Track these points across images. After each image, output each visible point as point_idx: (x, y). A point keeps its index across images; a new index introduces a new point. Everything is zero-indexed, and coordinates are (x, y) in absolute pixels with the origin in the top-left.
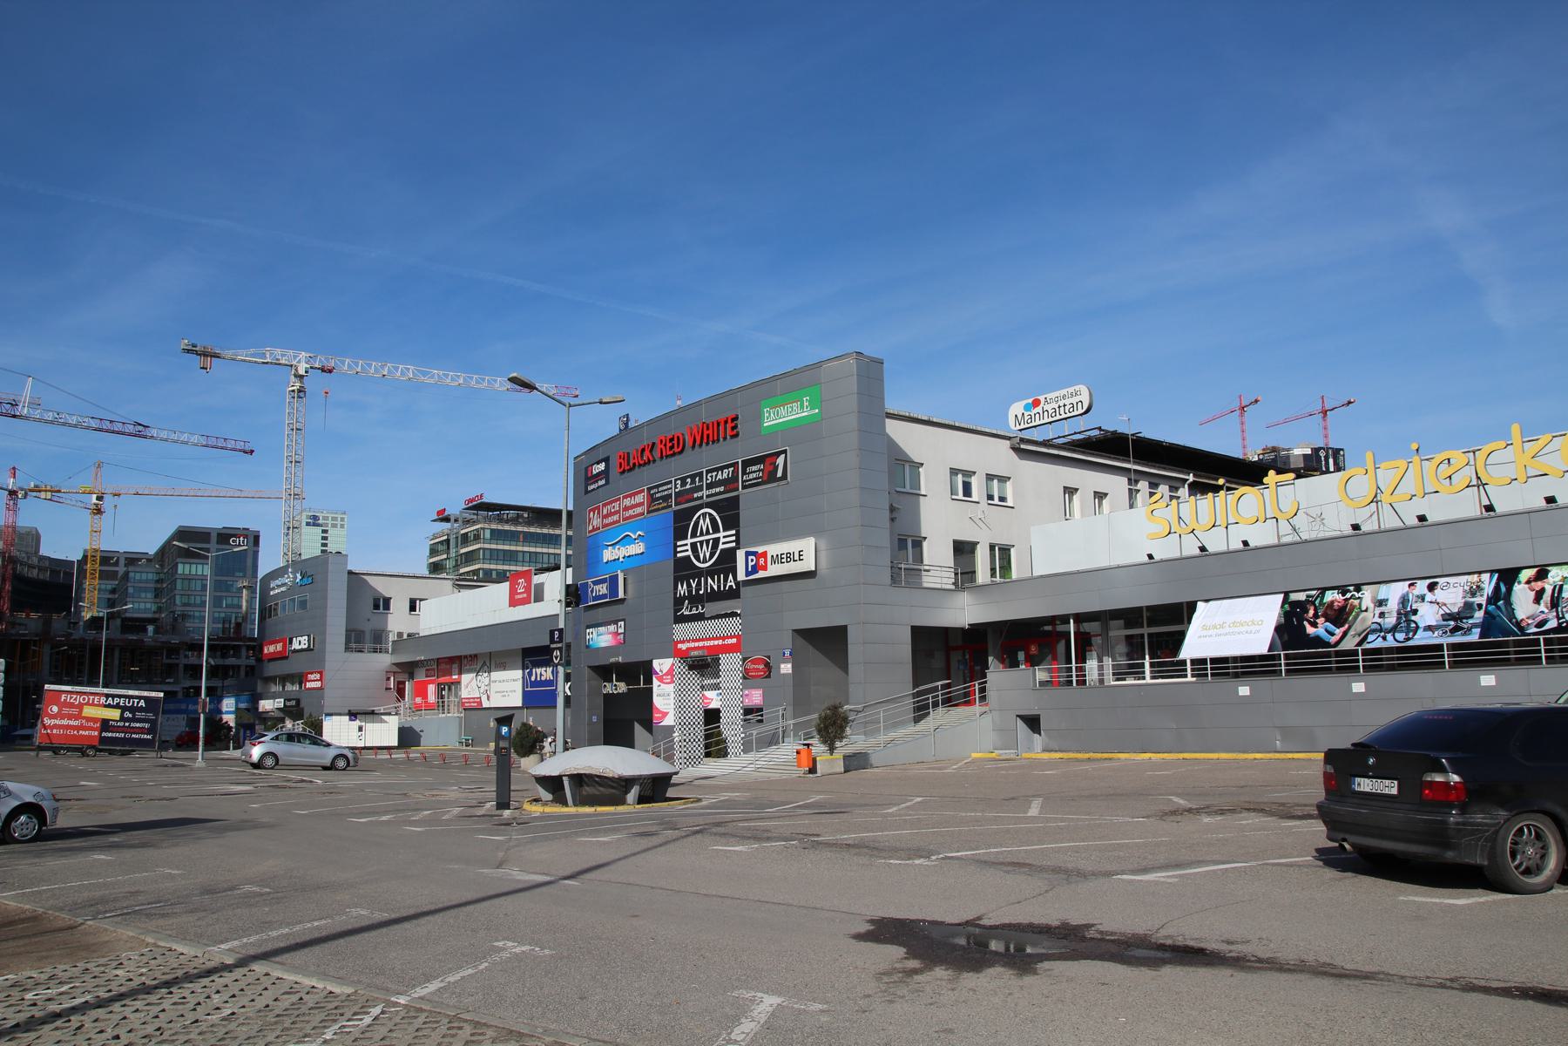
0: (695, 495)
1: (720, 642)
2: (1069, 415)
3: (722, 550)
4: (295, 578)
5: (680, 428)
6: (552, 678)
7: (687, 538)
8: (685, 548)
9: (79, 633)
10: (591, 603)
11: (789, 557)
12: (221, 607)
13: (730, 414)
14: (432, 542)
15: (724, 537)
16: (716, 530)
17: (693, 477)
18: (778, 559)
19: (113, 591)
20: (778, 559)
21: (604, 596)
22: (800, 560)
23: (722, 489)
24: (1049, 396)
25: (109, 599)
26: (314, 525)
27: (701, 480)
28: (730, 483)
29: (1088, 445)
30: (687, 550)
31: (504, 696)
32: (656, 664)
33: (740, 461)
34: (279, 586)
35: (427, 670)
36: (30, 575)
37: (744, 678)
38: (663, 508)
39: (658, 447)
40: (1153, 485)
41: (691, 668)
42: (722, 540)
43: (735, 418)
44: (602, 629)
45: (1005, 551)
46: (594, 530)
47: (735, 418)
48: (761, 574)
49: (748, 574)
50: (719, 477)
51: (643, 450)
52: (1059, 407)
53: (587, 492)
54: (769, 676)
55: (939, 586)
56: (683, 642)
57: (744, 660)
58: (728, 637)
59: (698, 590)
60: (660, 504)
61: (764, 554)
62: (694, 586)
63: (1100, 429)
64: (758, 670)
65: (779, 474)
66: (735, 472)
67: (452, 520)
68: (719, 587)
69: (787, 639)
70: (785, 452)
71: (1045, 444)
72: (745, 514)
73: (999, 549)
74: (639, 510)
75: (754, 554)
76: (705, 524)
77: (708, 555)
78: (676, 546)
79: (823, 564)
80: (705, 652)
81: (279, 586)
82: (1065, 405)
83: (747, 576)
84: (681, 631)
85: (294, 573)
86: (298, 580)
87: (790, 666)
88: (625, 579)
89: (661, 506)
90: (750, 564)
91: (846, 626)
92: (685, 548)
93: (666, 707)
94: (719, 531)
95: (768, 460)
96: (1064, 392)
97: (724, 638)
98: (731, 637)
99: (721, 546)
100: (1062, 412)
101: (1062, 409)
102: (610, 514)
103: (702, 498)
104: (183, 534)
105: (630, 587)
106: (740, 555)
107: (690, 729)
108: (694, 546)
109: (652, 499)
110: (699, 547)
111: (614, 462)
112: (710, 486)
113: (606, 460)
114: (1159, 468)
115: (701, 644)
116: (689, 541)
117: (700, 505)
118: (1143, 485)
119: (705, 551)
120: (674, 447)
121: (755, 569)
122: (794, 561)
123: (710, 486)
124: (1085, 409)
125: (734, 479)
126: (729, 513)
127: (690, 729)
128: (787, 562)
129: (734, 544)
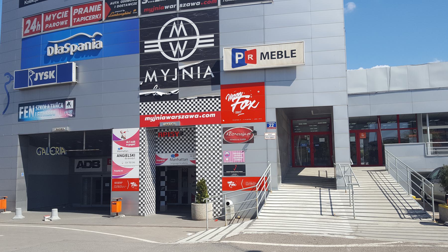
6: (53, 77)
7: (156, 38)
10: (32, 86)
15: (200, 39)
21: (52, 80)
22: (292, 56)
30: (158, 48)
32: (116, 132)
42: (198, 41)
49: (234, 65)
60: (123, 12)
62: (165, 74)
68: (195, 76)
78: (143, 45)
80: (178, 124)
88: (76, 67)
89: (123, 14)
90: (237, 59)
91: (332, 106)
93: (129, 164)
99: (197, 46)
103: (175, 9)
105: (80, 74)
107: (214, 194)
121: (242, 63)
122: (286, 57)
127: (214, 194)
128: (278, 58)
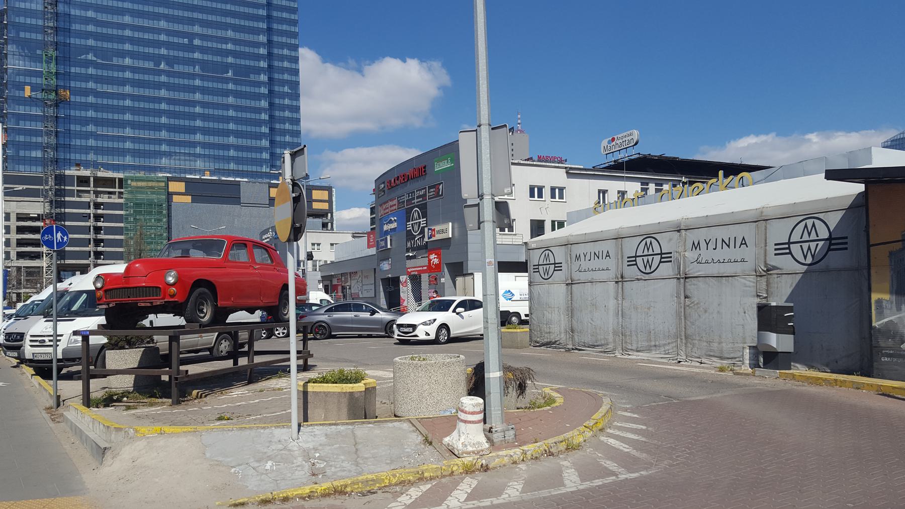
1: (421, 268)
2: (627, 146)
4: (273, 234)
13: (423, 165)
14: (371, 206)
16: (420, 219)
17: (412, 193)
18: (439, 232)
20: (439, 232)
21: (383, 247)
23: (421, 199)
24: (619, 136)
27: (414, 195)
29: (610, 168)
31: (367, 292)
34: (266, 239)
35: (338, 279)
37: (429, 284)
40: (659, 184)
42: (422, 223)
44: (385, 262)
47: (425, 167)
49: (429, 238)
52: (623, 142)
53: (379, 198)
55: (511, 243)
56: (409, 268)
57: (429, 276)
65: (440, 194)
66: (426, 191)
71: (594, 169)
73: (558, 222)
74: (394, 207)
75: (431, 229)
76: (416, 215)
79: (456, 234)
81: (266, 239)
82: (625, 141)
83: (428, 239)
84: (410, 263)
90: (430, 234)
94: (420, 219)
95: (436, 186)
96: (625, 134)
97: (422, 267)
99: (421, 226)
100: (624, 145)
101: (624, 142)
105: (393, 242)
106: (426, 229)
109: (399, 203)
112: (418, 198)
113: (384, 183)
115: (415, 269)
116: (411, 223)
117: (414, 206)
119: (416, 228)
123: (418, 198)
124: (634, 143)
125: (425, 195)
129: (425, 225)
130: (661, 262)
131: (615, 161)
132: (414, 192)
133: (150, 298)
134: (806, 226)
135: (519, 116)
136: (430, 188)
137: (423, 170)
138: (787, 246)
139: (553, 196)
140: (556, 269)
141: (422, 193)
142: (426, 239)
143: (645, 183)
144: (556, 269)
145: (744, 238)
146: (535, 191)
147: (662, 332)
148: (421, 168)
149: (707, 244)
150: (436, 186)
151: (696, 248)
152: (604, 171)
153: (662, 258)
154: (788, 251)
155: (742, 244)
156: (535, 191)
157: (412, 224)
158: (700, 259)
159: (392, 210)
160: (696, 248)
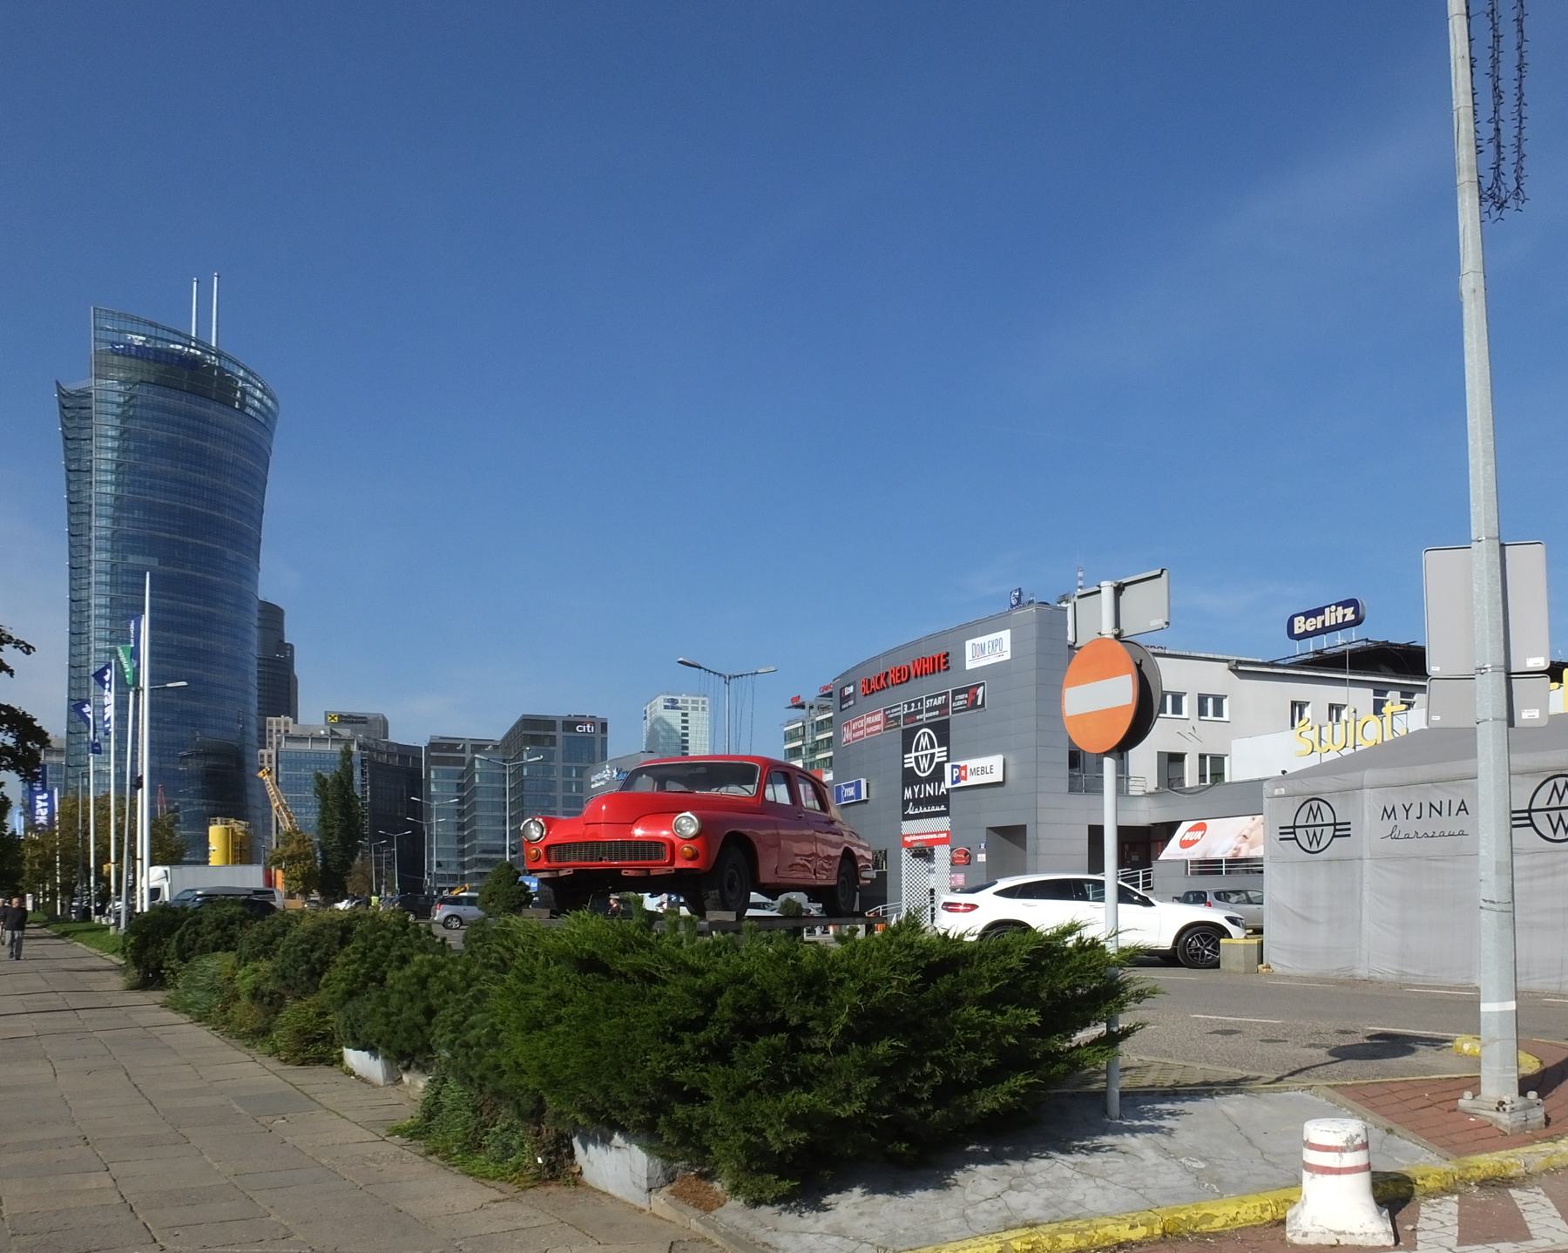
0: (918, 717)
3: (937, 763)
4: (612, 773)
5: (905, 661)
7: (911, 752)
8: (910, 761)
9: (1050, 1003)
11: (983, 771)
12: (571, 791)
16: (933, 746)
17: (916, 702)
19: (461, 777)
21: (852, 798)
23: (937, 713)
25: (458, 784)
26: (673, 708)
27: (922, 705)
28: (944, 706)
33: (950, 690)
36: (380, 760)
37: (952, 864)
38: (895, 727)
39: (891, 676)
41: (914, 856)
42: (937, 755)
43: (947, 655)
45: (1218, 761)
46: (847, 742)
47: (947, 655)
48: (963, 783)
49: (953, 783)
50: (935, 703)
51: (879, 678)
53: (841, 710)
54: (969, 864)
56: (908, 835)
57: (952, 850)
58: (941, 832)
59: (919, 795)
61: (965, 768)
63: (1367, 640)
64: (961, 859)
65: (979, 703)
67: (807, 706)
69: (983, 833)
70: (983, 684)
71: (1272, 664)
72: (954, 735)
74: (877, 727)
75: (958, 767)
76: (924, 741)
77: (926, 767)
78: (903, 759)
84: (908, 827)
85: (610, 769)
86: (614, 776)
87: (984, 855)
90: (955, 775)
92: (910, 761)
95: (970, 690)
97: (937, 833)
98: (943, 832)
99: (936, 760)
102: (858, 730)
104: (528, 722)
106: (948, 767)
108: (916, 758)
109: (887, 719)
110: (920, 759)
111: (860, 686)
112: (928, 710)
114: (1412, 679)
116: (913, 754)
118: (1393, 696)
119: (924, 763)
120: (903, 676)
121: (958, 779)
123: (928, 710)
126: (942, 732)
130: (1334, 836)
131: (1316, 652)
132: (921, 700)
133: (650, 862)
134: (1555, 787)
135: (1080, 574)
136: (956, 693)
137: (942, 660)
138: (1292, 830)
139: (1202, 711)
140: (1337, 833)
141: (939, 701)
142: (948, 784)
143: (1380, 690)
144: (1337, 833)
145: (1463, 802)
146: (270, 756)
147: (348, 1035)
148: (939, 658)
149: (1407, 811)
150: (970, 690)
151: (1389, 817)
152: (1296, 668)
153: (1336, 830)
154: (1293, 836)
155: (1460, 810)
156: (270, 756)
157: (916, 758)
158: (1397, 833)
159: (872, 733)
160: (1389, 817)
